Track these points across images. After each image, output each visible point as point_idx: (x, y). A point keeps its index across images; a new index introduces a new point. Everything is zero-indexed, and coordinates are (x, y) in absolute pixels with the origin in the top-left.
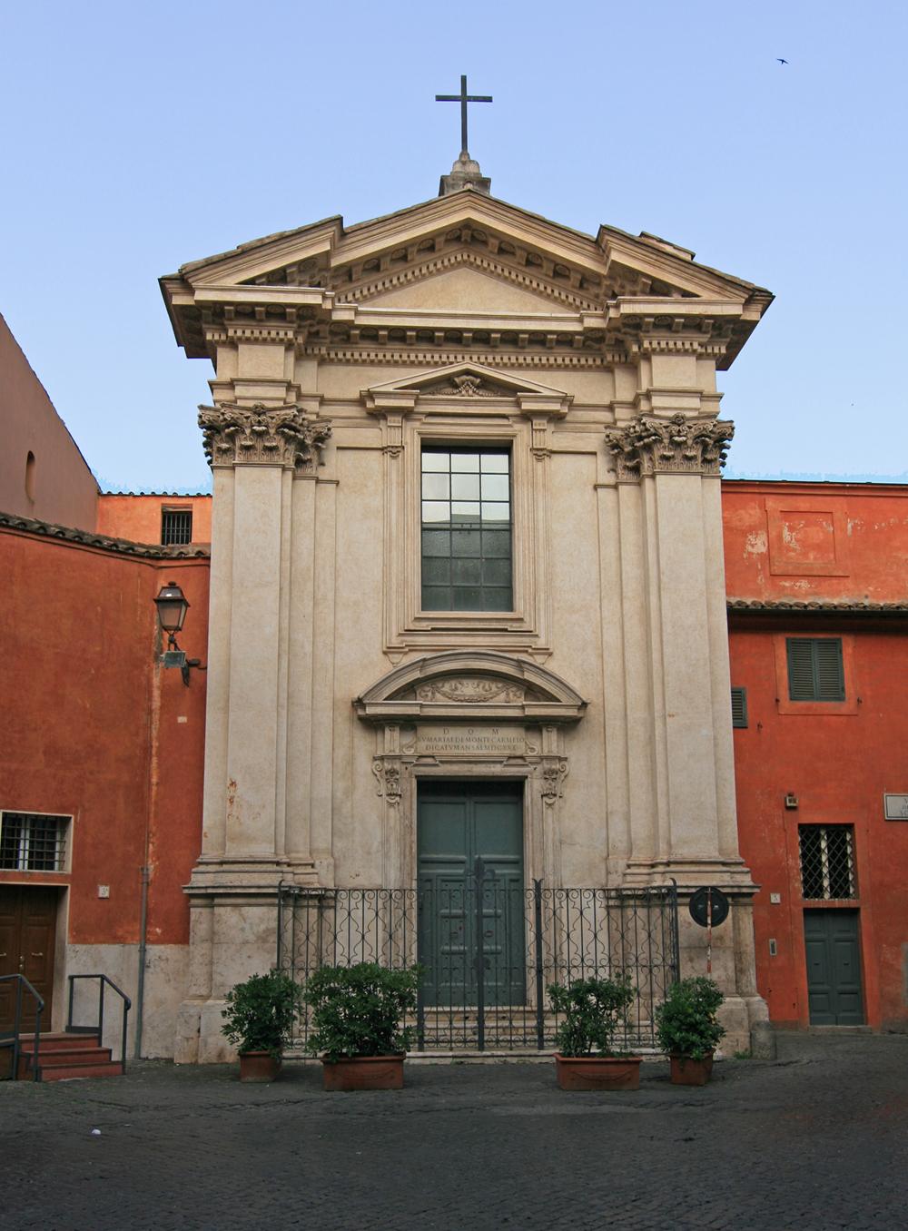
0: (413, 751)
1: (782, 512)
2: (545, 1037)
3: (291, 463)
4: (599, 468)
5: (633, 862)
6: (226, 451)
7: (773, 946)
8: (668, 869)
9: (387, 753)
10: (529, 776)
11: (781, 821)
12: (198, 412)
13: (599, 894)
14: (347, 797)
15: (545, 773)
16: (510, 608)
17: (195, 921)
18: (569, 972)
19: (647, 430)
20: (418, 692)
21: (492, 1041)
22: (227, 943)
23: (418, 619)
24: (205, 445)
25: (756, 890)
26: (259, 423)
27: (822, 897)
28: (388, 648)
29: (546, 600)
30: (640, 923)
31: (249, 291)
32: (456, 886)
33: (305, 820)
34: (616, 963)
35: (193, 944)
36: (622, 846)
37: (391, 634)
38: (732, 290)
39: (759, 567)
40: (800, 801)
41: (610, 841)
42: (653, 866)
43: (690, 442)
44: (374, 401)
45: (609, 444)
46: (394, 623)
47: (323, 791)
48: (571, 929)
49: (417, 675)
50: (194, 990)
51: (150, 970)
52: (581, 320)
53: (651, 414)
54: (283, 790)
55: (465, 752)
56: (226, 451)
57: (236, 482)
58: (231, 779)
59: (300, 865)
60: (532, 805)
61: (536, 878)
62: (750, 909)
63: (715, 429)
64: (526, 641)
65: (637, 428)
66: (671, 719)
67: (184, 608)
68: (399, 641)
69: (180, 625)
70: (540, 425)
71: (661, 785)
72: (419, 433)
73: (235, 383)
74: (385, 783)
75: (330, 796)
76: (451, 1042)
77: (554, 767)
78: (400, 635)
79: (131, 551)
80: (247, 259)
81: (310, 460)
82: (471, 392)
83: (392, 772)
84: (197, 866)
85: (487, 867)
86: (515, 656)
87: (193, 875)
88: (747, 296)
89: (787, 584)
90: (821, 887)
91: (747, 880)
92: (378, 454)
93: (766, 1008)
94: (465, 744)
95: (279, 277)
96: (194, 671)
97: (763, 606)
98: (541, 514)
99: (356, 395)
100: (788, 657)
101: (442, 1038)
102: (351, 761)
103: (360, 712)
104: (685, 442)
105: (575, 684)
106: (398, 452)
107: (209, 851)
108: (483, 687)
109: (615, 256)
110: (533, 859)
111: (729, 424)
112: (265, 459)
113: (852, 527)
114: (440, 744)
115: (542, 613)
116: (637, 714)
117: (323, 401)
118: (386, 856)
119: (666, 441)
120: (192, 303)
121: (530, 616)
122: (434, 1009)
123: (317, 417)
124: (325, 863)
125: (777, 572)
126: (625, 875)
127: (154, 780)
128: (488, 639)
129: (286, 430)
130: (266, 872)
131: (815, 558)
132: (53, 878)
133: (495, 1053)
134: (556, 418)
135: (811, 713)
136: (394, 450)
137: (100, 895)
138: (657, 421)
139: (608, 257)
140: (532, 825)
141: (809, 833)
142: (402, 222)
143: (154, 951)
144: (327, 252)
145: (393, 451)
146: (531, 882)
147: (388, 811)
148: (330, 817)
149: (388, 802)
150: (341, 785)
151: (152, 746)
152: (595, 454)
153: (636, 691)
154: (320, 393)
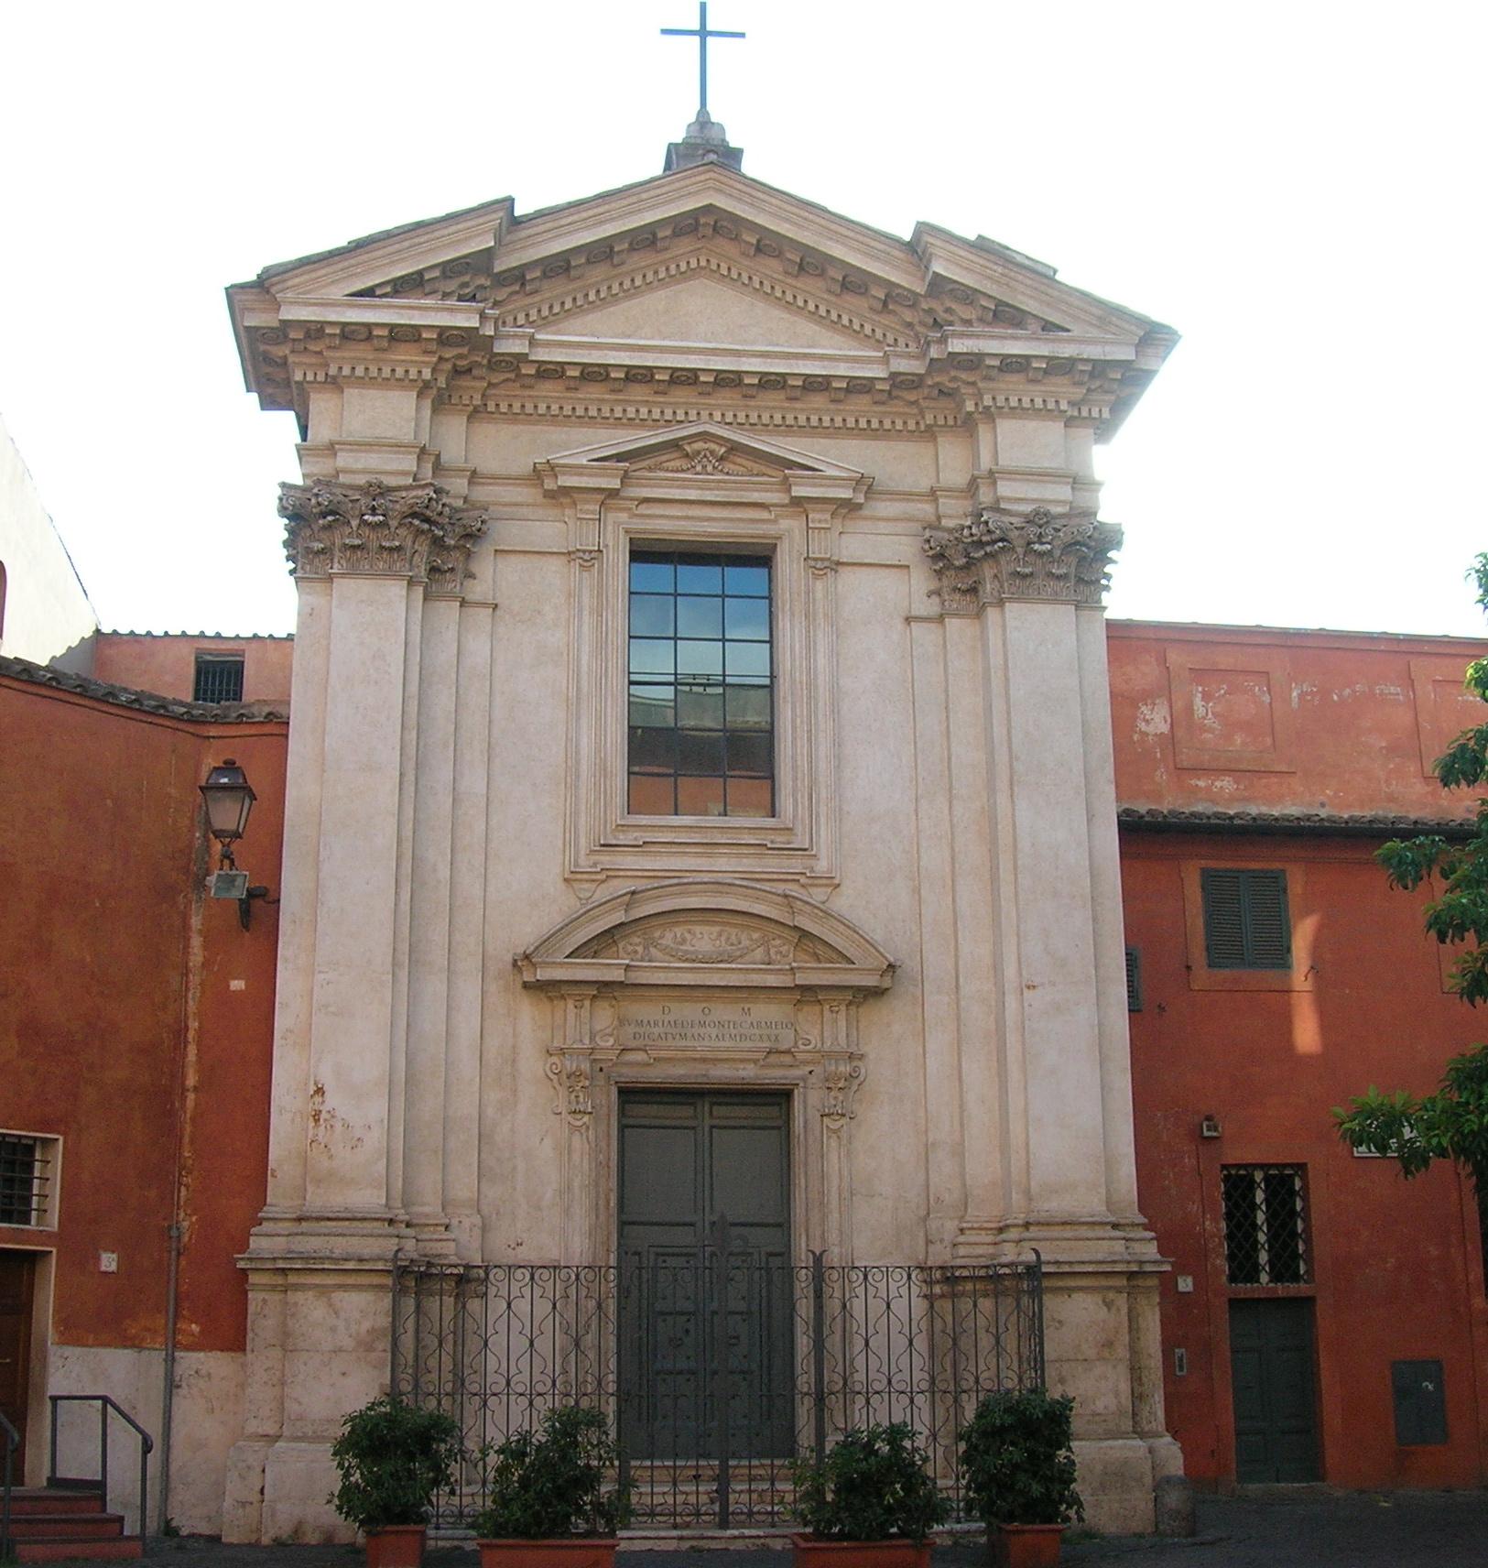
3: (422, 571)
4: (916, 588)
7: (1181, 1359)
8: (1027, 1235)
20: (621, 946)
21: (742, 1513)
24: (286, 544)
26: (374, 511)
27: (1258, 1281)
30: (982, 1322)
31: (365, 306)
32: (681, 1262)
33: (436, 1152)
34: (943, 1386)
37: (577, 853)
43: (1057, 553)
45: (931, 553)
47: (465, 1105)
48: (871, 1331)
49: (618, 917)
50: (253, 1426)
51: (184, 1391)
52: (885, 360)
53: (996, 509)
54: (400, 1103)
58: (316, 1084)
60: (806, 1132)
64: (796, 865)
69: (240, 830)
76: (674, 1514)
79: (162, 711)
80: (365, 257)
82: (710, 468)
85: (735, 1231)
86: (781, 887)
87: (252, 1239)
89: (1202, 783)
90: (1256, 1264)
91: (1150, 1250)
92: (555, 564)
93: (1180, 1455)
94: (696, 1031)
95: (401, 287)
97: (1165, 817)
100: (1203, 897)
101: (659, 1509)
103: (528, 977)
107: (279, 1197)
110: (807, 1221)
113: (1299, 695)
114: (656, 1030)
117: (474, 477)
119: (1020, 550)
123: (465, 502)
124: (467, 1223)
125: (1185, 764)
127: (191, 1081)
129: (416, 522)
130: (372, 1236)
132: (30, 1236)
133: (747, 1532)
136: (587, 557)
137: (103, 1269)
138: (1007, 519)
139: (927, 268)
140: (806, 1164)
141: (1238, 1185)
143: (189, 1361)
147: (570, 1139)
151: (187, 1028)
154: (471, 466)
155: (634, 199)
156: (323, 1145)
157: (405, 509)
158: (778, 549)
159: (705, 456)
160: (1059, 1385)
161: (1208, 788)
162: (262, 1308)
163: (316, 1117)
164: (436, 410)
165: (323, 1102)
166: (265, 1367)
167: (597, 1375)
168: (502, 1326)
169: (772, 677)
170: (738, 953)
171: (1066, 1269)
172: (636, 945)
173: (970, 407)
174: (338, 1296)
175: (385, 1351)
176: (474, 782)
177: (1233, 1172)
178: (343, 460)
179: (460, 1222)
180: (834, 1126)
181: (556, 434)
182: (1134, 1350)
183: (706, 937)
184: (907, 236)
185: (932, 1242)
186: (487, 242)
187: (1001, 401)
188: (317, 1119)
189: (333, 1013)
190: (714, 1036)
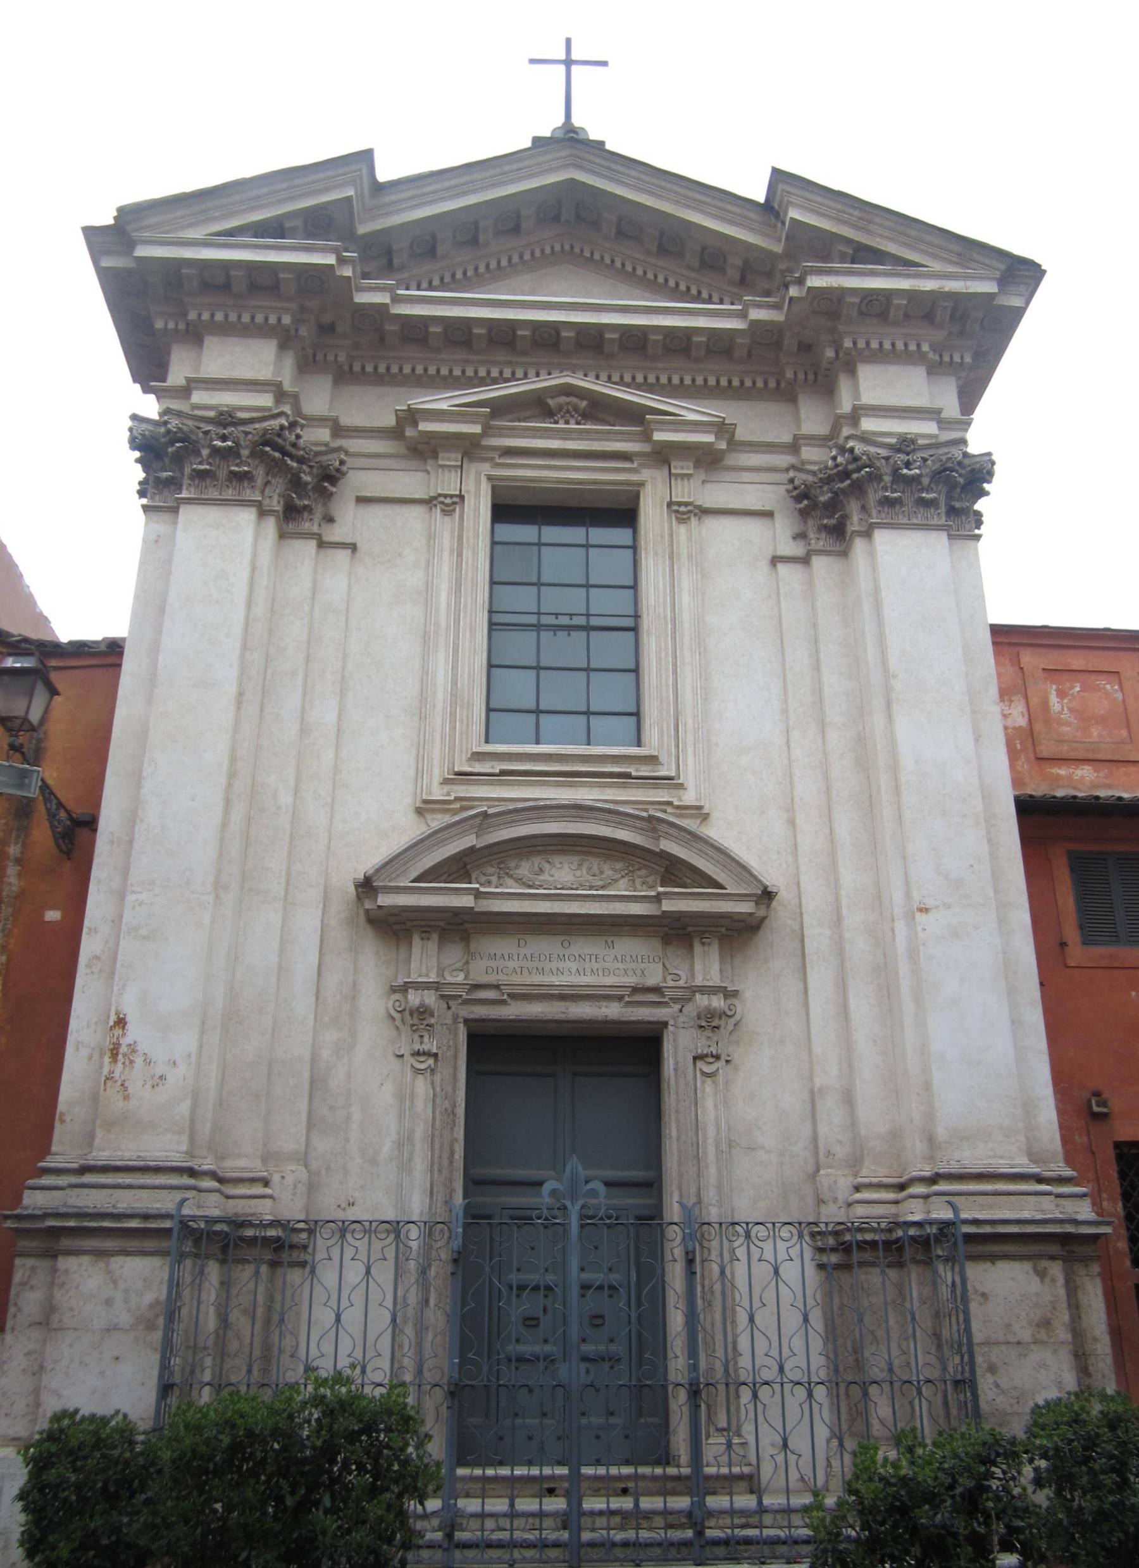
3: (277, 505)
5: (866, 1180)
9: (414, 978)
10: (671, 1022)
12: (130, 423)
15: (699, 1017)
18: (755, 1396)
19: (856, 459)
22: (75, 1329)
23: (478, 756)
25: (1107, 1230)
26: (224, 438)
28: (425, 802)
36: (840, 1152)
38: (980, 258)
39: (1019, 747)
40: (1117, 1103)
42: (902, 1187)
43: (926, 481)
45: (795, 493)
46: (436, 762)
52: (743, 315)
55: (556, 980)
58: (117, 1013)
61: (685, 1201)
62: (1096, 1268)
64: (662, 796)
65: (840, 459)
68: (445, 791)
70: (682, 468)
72: (490, 478)
73: (193, 385)
74: (410, 1032)
75: (307, 1056)
81: (306, 508)
83: (423, 1012)
84: (39, 1176)
87: (27, 1193)
91: (1084, 1211)
95: (274, 229)
99: (390, 421)
102: (353, 995)
103: (368, 905)
104: (916, 479)
106: (454, 503)
108: (589, 869)
109: (794, 214)
110: (681, 1175)
112: (229, 493)
114: (511, 964)
115: (690, 750)
117: (338, 430)
118: (405, 1167)
119: (887, 479)
121: (669, 754)
122: (504, 1471)
124: (289, 1180)
125: (1045, 754)
126: (849, 1205)
129: (268, 449)
135: (1116, 964)
136: (448, 501)
138: (872, 450)
145: (450, 504)
146: (676, 1206)
149: (412, 1066)
150: (330, 1037)
152: (769, 515)
155: (498, 171)
156: (119, 1083)
157: (256, 438)
160: (988, 1375)
162: (29, 1277)
163: (114, 1053)
170: (601, 883)
171: (987, 1229)
172: (491, 875)
173: (830, 353)
174: (117, 1262)
176: (325, 713)
178: (198, 397)
179: (283, 1177)
182: (1077, 1332)
184: (759, 195)
185: (824, 1202)
187: (861, 344)
188: (114, 1055)
189: (144, 938)
190: (574, 971)
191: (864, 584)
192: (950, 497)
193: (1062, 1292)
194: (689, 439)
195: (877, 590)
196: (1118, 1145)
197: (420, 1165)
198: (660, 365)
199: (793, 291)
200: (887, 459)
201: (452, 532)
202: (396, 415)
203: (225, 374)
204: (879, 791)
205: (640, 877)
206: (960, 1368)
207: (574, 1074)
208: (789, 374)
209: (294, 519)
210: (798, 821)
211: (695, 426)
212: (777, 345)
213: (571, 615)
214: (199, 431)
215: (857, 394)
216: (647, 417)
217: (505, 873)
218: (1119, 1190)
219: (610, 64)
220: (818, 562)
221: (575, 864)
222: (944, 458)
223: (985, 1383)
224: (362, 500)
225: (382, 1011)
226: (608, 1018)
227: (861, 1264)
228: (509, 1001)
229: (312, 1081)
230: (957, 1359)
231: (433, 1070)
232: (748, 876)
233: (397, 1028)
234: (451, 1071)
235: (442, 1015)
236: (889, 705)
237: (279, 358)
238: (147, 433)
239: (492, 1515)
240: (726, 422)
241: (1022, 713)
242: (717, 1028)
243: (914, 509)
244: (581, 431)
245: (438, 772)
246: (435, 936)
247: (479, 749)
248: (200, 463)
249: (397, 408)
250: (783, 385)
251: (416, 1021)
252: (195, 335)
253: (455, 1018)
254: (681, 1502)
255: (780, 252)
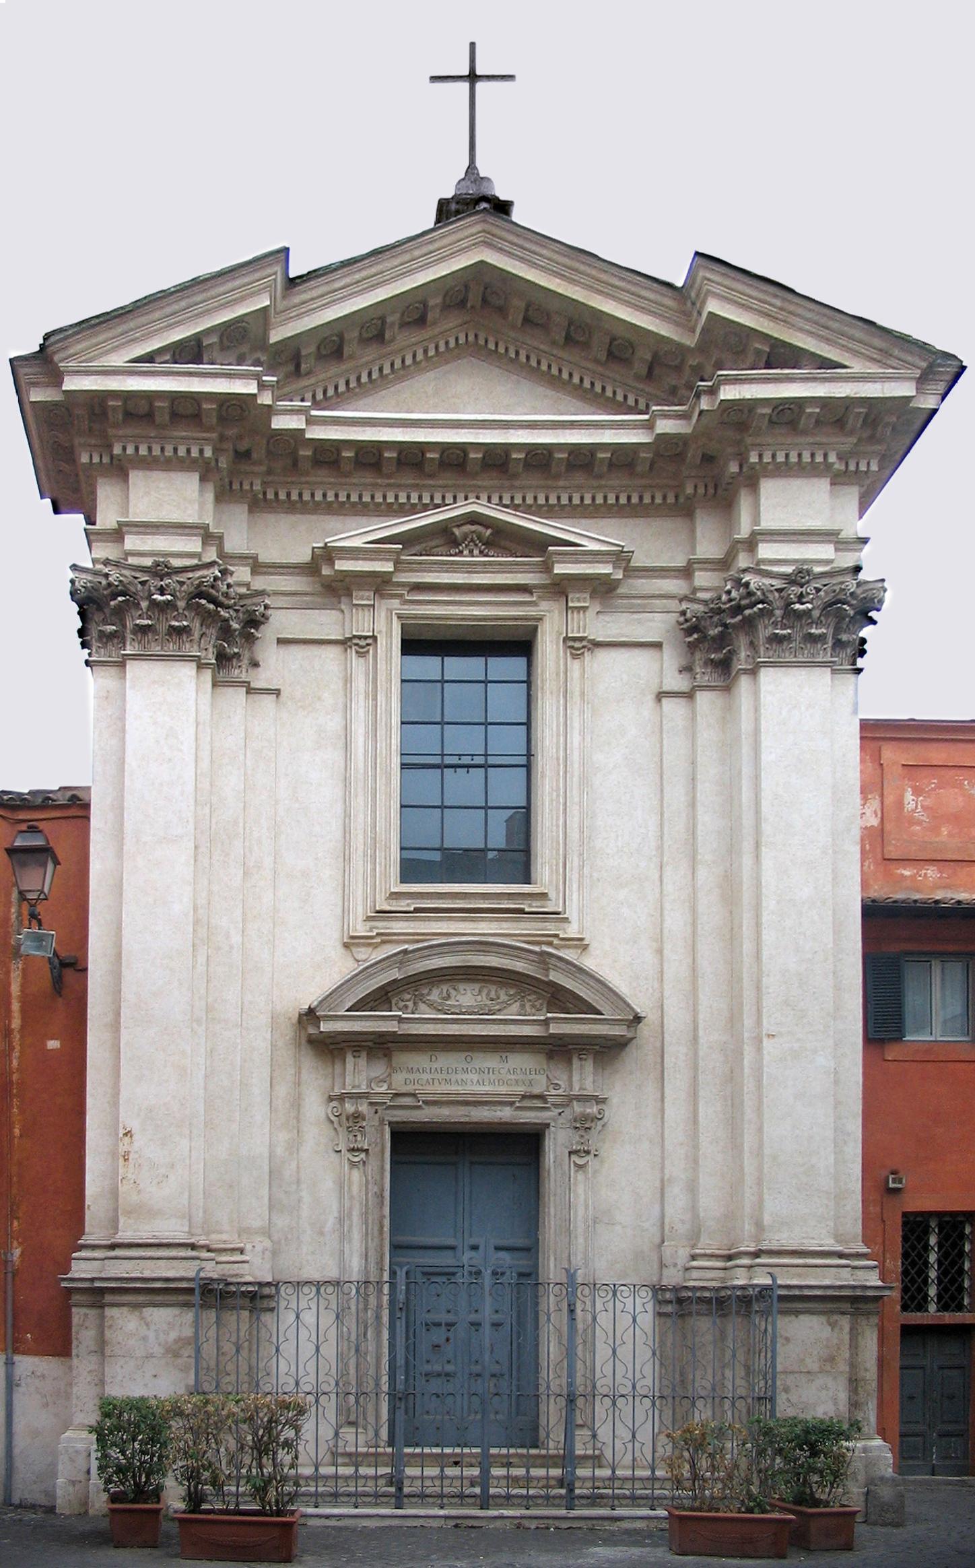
0: (385, 1086)
1: (903, 765)
2: (577, 1492)
5: (703, 1251)
6: (112, 636)
9: (349, 1089)
10: (552, 1124)
11: (878, 1209)
12: (71, 575)
13: (646, 1294)
14: (291, 1154)
16: (527, 880)
17: (78, 1325)
19: (750, 594)
20: (394, 1002)
25: (886, 1293)
26: (162, 591)
28: (353, 937)
29: (582, 867)
35: (78, 1356)
36: (682, 1229)
41: (667, 1220)
42: (730, 1258)
43: (816, 613)
44: (333, 564)
45: (685, 626)
46: (360, 902)
49: (396, 974)
51: (21, 1389)
52: (649, 426)
55: (460, 1089)
56: (112, 636)
57: (128, 684)
59: (225, 1250)
62: (875, 1320)
63: (859, 591)
64: (551, 928)
65: (734, 594)
66: (772, 1041)
67: (50, 867)
71: (748, 1141)
72: (400, 617)
73: (124, 529)
75: (266, 1155)
77: (588, 1111)
78: (369, 919)
80: (143, 320)
81: (237, 655)
82: (476, 552)
83: (357, 1117)
88: (924, 364)
89: (907, 873)
92: (333, 652)
96: (69, 974)
98: (575, 739)
99: (304, 556)
103: (312, 1030)
104: (808, 613)
105: (623, 988)
106: (368, 645)
107: (94, 1232)
108: (488, 994)
109: (713, 306)
111: (880, 585)
112: (171, 648)
114: (425, 1076)
116: (710, 1037)
117: (258, 568)
118: (343, 1237)
119: (778, 613)
120: (58, 397)
126: (687, 1269)
128: (494, 925)
129: (203, 602)
131: (950, 835)
133: (506, 1513)
134: (602, 589)
138: (767, 581)
142: (379, 268)
144: (265, 309)
145: (359, 644)
148: (267, 1182)
149: (349, 1159)
152: (657, 645)
153: (711, 1002)
157: (192, 589)
158: (539, 630)
159: (472, 540)
161: (913, 877)
164: (219, 499)
165: (132, 1142)
166: (88, 1370)
167: (631, 1427)
168: (291, 1334)
169: (529, 755)
170: (497, 1007)
171: (797, 1292)
173: (734, 468)
174: (148, 1311)
175: (189, 1357)
177: (912, 1219)
180: (580, 1161)
181: (332, 522)
182: (853, 1365)
183: (469, 991)
186: (263, 302)
191: (746, 725)
192: (837, 630)
193: (847, 1337)
194: (588, 571)
195: (757, 731)
196: (905, 1214)
197: (356, 1236)
198: (561, 483)
199: (705, 403)
200: (780, 590)
201: (367, 675)
202: (313, 552)
203: (152, 517)
204: (741, 927)
205: (530, 1001)
206: (763, 1389)
207: (472, 1163)
208: (689, 490)
209: (224, 667)
210: (665, 951)
211: (595, 556)
212: (679, 457)
213: (473, 755)
214: (136, 581)
215: (756, 518)
216: (550, 548)
217: (419, 999)
218: (900, 1250)
219: (517, 78)
220: (703, 698)
221: (477, 990)
222: (837, 588)
223: (781, 1399)
224: (281, 642)
225: (323, 1115)
226: (503, 1120)
227: (698, 1314)
228: (424, 1106)
229: (270, 1172)
230: (762, 1383)
231: (364, 1162)
232: (622, 1003)
233: (335, 1129)
234: (379, 1163)
235: (370, 1123)
236: (757, 845)
237: (201, 491)
238: (89, 584)
239: (641, 1479)
240: (625, 550)
241: (875, 812)
242: (589, 1128)
243: (802, 645)
244: (484, 564)
245: (359, 910)
246: (364, 1054)
247: (396, 890)
248: (140, 617)
249: (315, 545)
250: (681, 500)
251: (351, 1124)
252: (120, 470)
253: (382, 1121)
254: (556, 1472)
255: (692, 346)
